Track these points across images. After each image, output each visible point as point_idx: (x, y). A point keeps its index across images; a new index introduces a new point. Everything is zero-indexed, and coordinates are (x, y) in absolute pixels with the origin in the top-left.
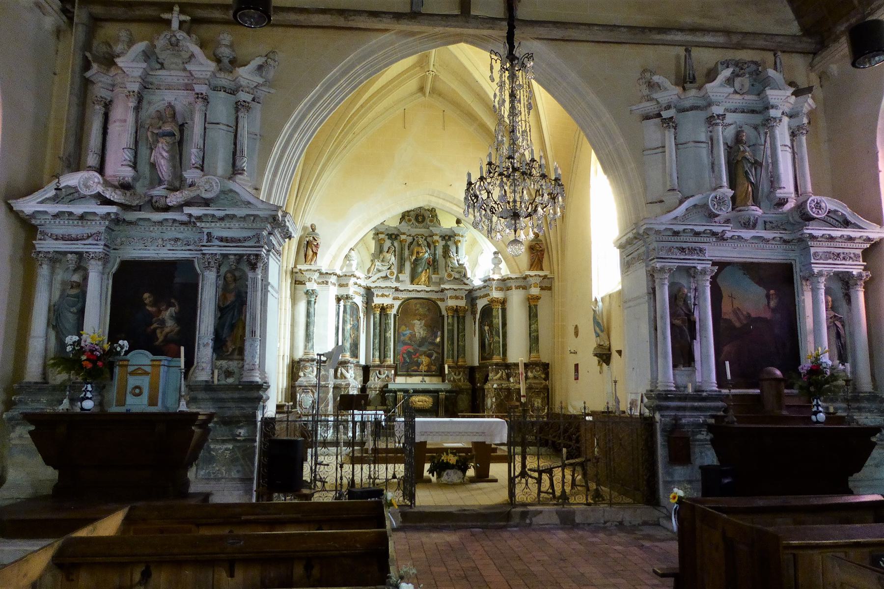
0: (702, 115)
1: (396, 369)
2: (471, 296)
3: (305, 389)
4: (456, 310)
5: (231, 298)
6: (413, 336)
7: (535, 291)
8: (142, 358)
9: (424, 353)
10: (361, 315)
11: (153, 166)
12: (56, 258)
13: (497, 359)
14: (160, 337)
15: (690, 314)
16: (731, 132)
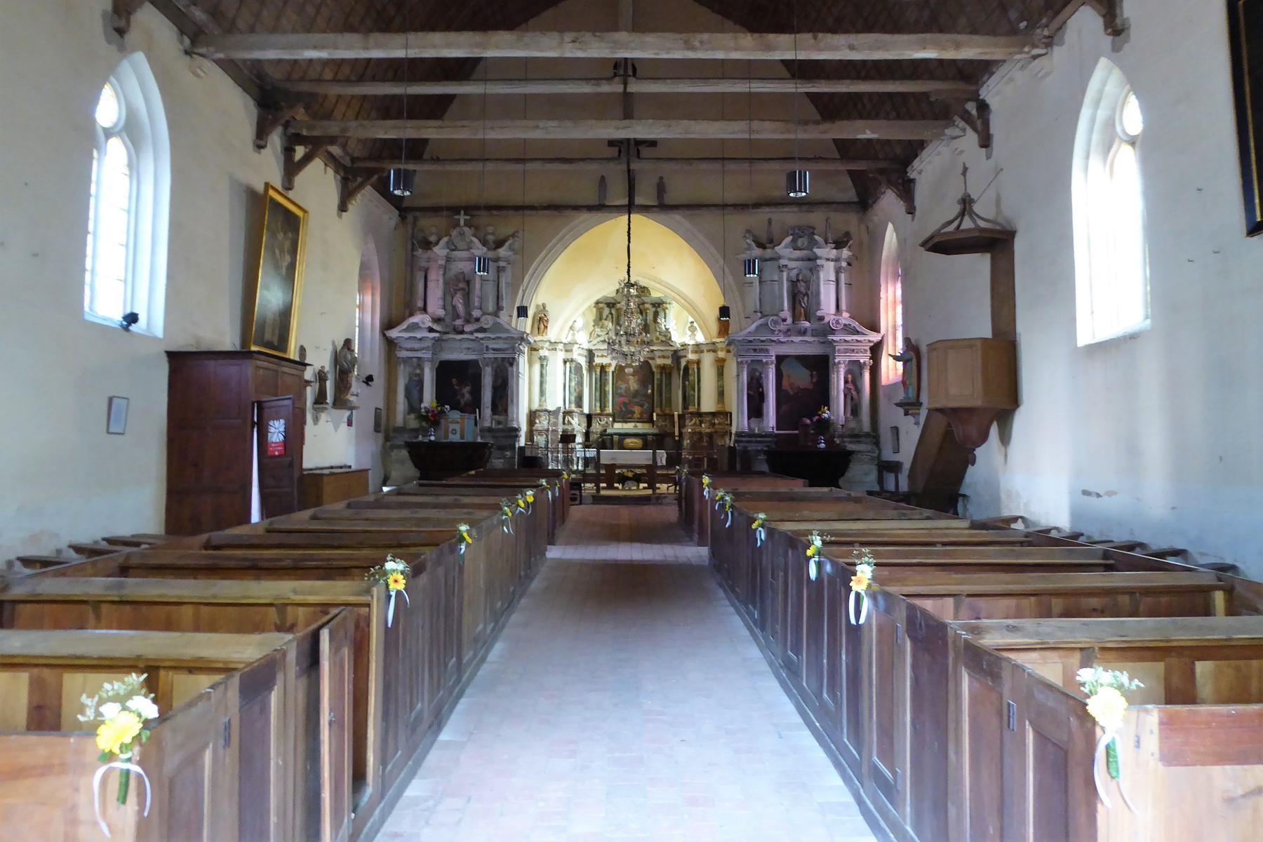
0: (775, 263)
1: (613, 416)
2: (677, 355)
3: (540, 432)
4: (663, 368)
5: (500, 381)
6: (628, 389)
7: (721, 354)
8: (456, 415)
9: (638, 404)
10: (585, 372)
11: (454, 307)
12: (406, 361)
13: (691, 409)
14: (462, 402)
15: (761, 386)
16: (794, 273)
